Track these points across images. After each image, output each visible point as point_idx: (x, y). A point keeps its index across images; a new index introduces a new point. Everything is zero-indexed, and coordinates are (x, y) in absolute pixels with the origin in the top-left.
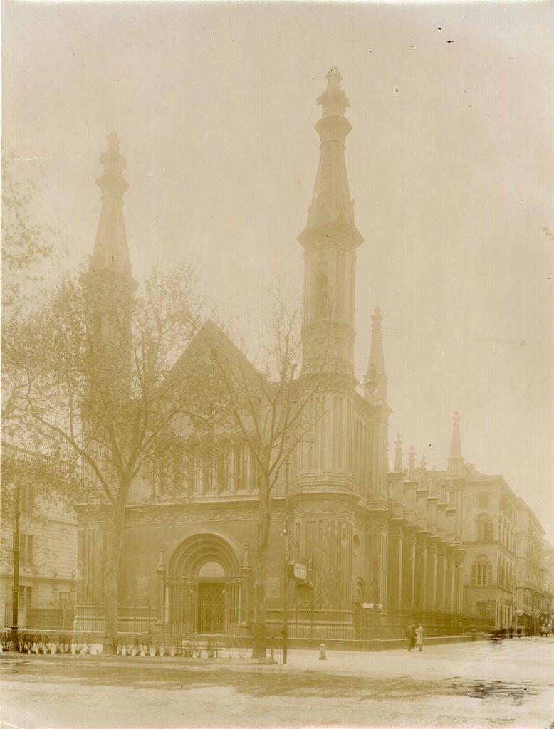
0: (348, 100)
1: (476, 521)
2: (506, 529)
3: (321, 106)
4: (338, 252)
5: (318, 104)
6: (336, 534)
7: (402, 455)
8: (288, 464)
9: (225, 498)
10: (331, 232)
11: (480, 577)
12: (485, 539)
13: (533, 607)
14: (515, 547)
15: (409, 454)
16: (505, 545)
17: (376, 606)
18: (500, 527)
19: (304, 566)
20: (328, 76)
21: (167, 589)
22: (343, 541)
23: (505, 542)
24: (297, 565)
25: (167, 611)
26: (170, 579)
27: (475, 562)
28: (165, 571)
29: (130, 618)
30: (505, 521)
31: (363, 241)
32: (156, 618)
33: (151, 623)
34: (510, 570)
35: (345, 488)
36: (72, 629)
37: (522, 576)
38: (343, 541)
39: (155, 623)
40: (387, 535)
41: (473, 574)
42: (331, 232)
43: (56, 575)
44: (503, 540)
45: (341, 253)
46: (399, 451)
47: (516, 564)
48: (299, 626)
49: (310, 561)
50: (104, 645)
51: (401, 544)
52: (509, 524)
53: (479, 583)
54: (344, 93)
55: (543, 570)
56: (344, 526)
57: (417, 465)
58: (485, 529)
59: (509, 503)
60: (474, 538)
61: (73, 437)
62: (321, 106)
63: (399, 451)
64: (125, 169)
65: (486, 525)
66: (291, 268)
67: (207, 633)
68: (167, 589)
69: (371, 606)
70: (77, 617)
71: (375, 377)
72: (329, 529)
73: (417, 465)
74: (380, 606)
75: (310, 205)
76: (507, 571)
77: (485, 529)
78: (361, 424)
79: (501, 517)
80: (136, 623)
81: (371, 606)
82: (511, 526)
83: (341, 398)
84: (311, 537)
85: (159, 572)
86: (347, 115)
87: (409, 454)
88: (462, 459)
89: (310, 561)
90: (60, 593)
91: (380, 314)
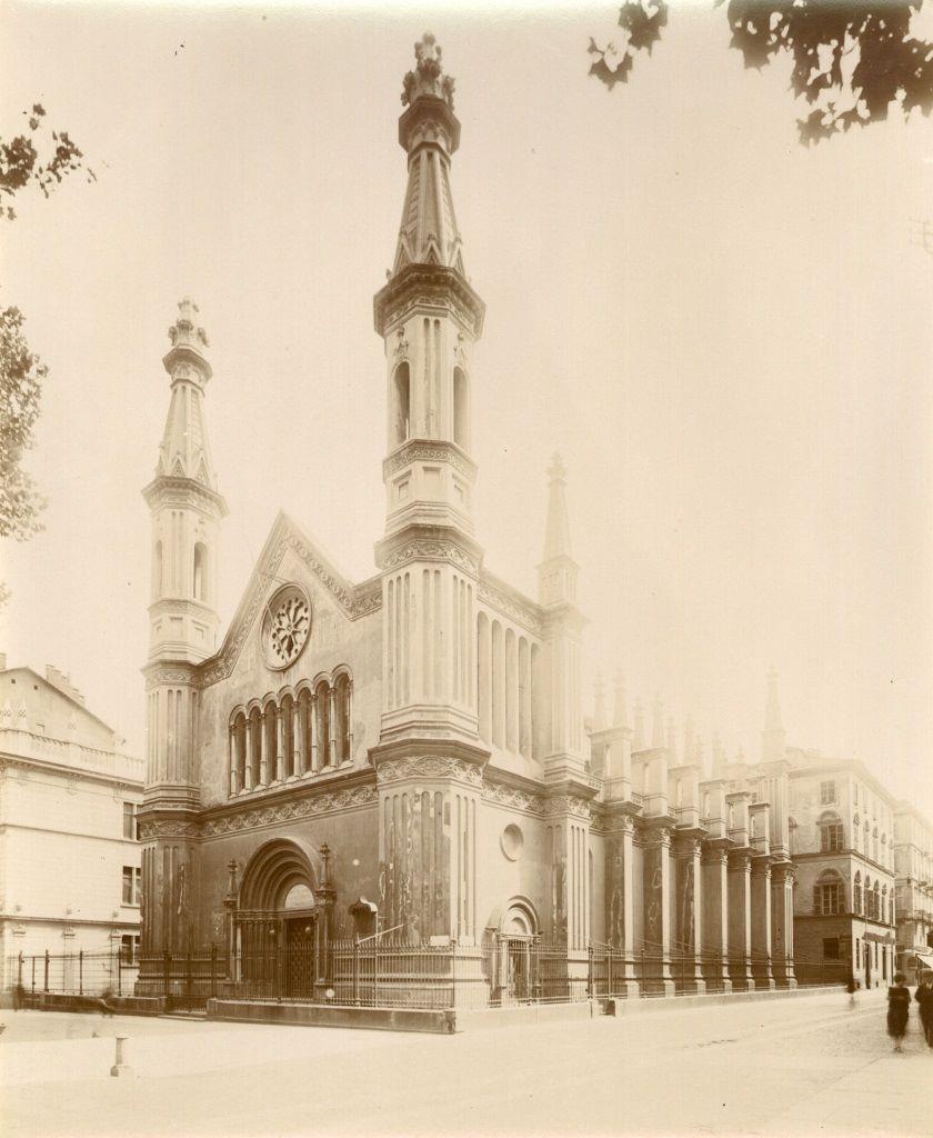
1: (818, 824)
4: (427, 321)
6: (432, 815)
11: (826, 903)
12: (833, 848)
21: (239, 931)
25: (239, 964)
26: (243, 914)
27: (818, 882)
28: (235, 903)
29: (410, 976)
32: (224, 975)
33: (218, 982)
39: (223, 982)
41: (817, 900)
48: (359, 984)
49: (391, 866)
60: (817, 849)
65: (832, 828)
68: (239, 931)
72: (418, 807)
76: (858, 889)
80: (401, 985)
85: (227, 904)
89: (391, 866)
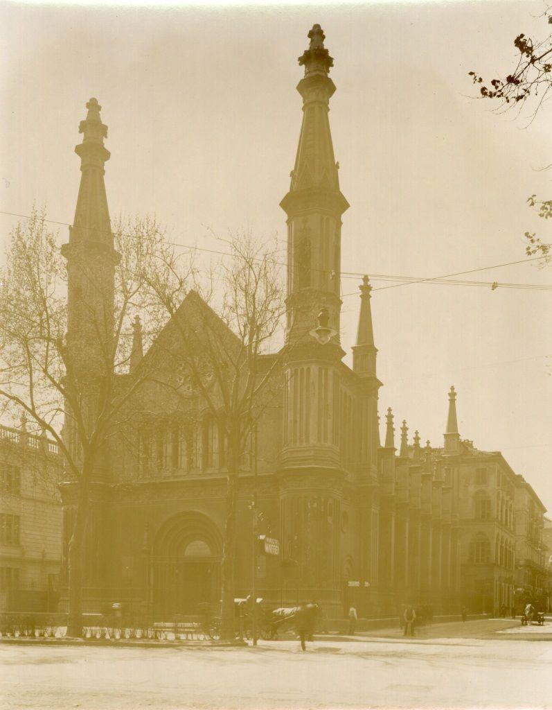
0: (332, 59)
2: (504, 506)
3: (304, 66)
5: (300, 64)
7: (394, 429)
8: (256, 432)
9: (211, 474)
10: (315, 197)
13: (534, 585)
14: (514, 525)
15: (414, 438)
16: (500, 519)
17: (362, 585)
18: (498, 504)
19: (277, 542)
20: (311, 35)
22: (329, 518)
23: (504, 520)
24: (270, 540)
30: (503, 497)
31: (348, 206)
34: (506, 545)
35: (331, 463)
36: (56, 611)
37: (522, 552)
38: (329, 518)
40: (378, 512)
42: (315, 197)
43: (44, 556)
44: (501, 518)
45: (325, 218)
46: (390, 424)
47: (516, 541)
50: (68, 627)
51: (393, 522)
52: (507, 501)
53: (477, 561)
54: (327, 51)
55: (544, 549)
56: (331, 501)
57: (423, 445)
58: (483, 505)
59: (515, 483)
61: (34, 408)
62: (304, 66)
63: (390, 424)
64: (106, 137)
66: (272, 233)
67: (440, 639)
69: (357, 584)
70: (61, 598)
71: (366, 350)
72: (315, 505)
73: (423, 445)
74: (367, 584)
75: (293, 169)
76: (506, 549)
77: (483, 505)
78: (503, 500)
79: (498, 494)
81: (357, 584)
82: (510, 503)
83: (326, 370)
84: (297, 514)
86: (330, 75)
87: (414, 438)
88: (459, 435)
89: (296, 538)
90: (49, 575)
91: (369, 283)
